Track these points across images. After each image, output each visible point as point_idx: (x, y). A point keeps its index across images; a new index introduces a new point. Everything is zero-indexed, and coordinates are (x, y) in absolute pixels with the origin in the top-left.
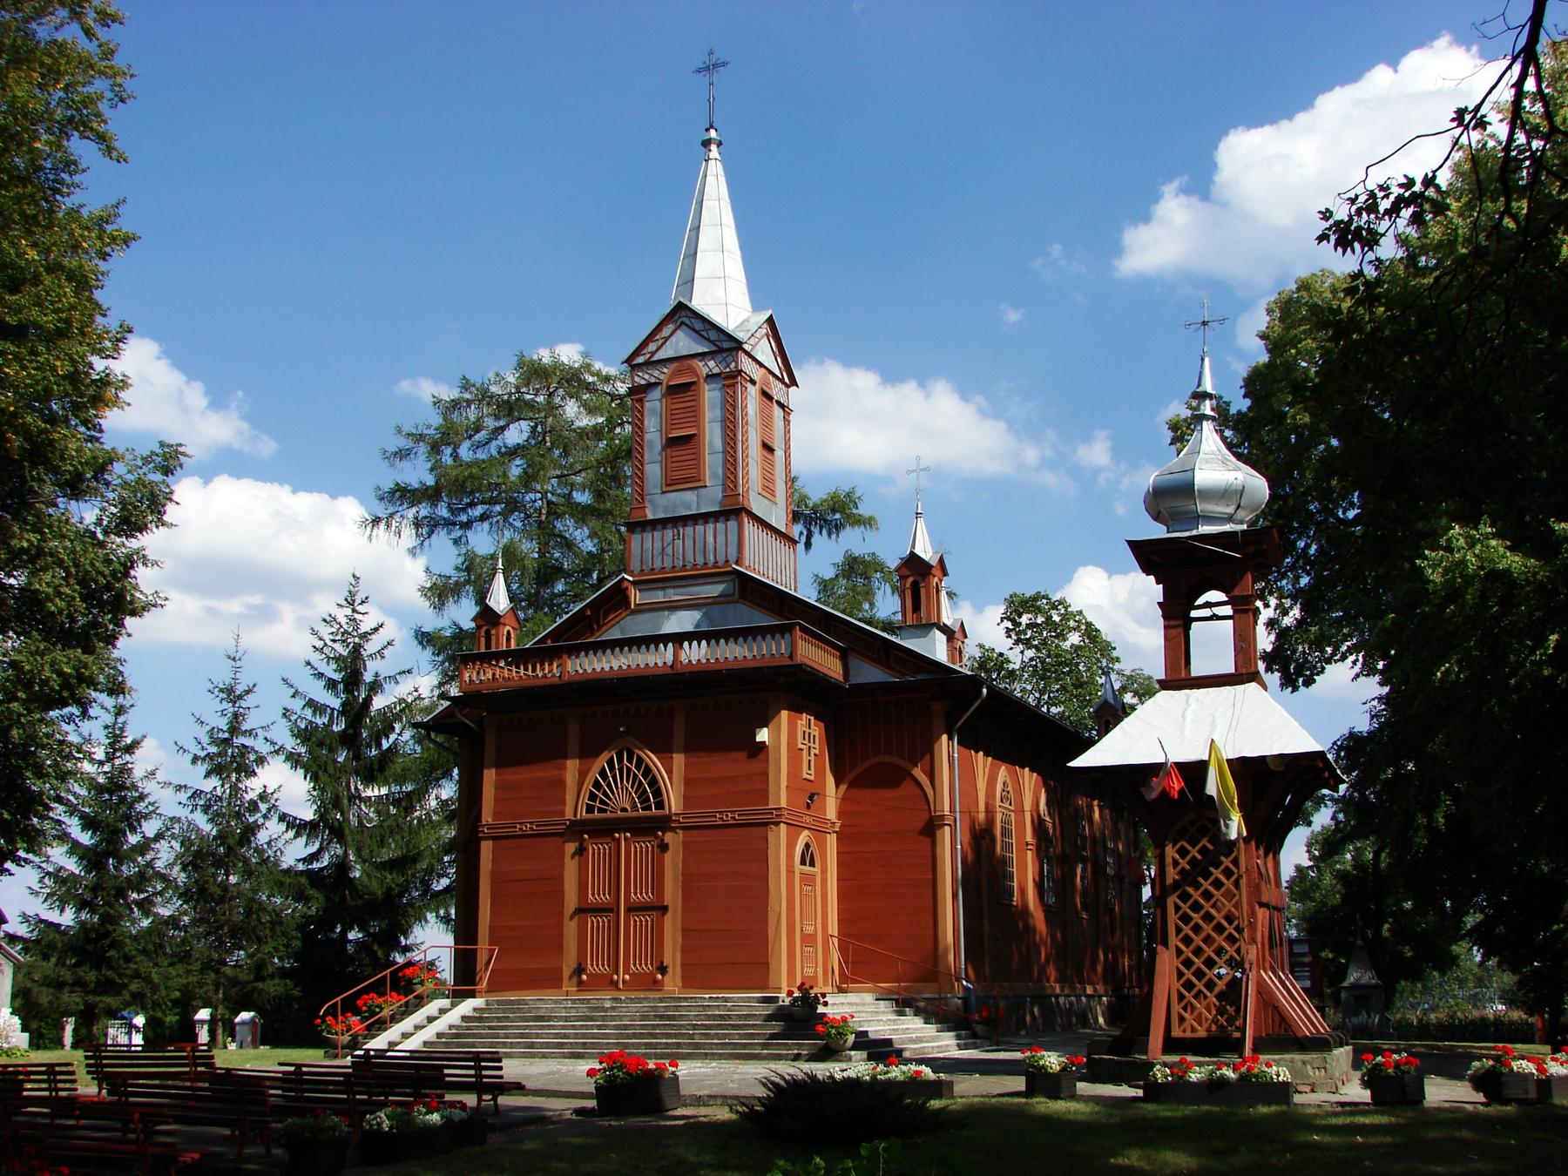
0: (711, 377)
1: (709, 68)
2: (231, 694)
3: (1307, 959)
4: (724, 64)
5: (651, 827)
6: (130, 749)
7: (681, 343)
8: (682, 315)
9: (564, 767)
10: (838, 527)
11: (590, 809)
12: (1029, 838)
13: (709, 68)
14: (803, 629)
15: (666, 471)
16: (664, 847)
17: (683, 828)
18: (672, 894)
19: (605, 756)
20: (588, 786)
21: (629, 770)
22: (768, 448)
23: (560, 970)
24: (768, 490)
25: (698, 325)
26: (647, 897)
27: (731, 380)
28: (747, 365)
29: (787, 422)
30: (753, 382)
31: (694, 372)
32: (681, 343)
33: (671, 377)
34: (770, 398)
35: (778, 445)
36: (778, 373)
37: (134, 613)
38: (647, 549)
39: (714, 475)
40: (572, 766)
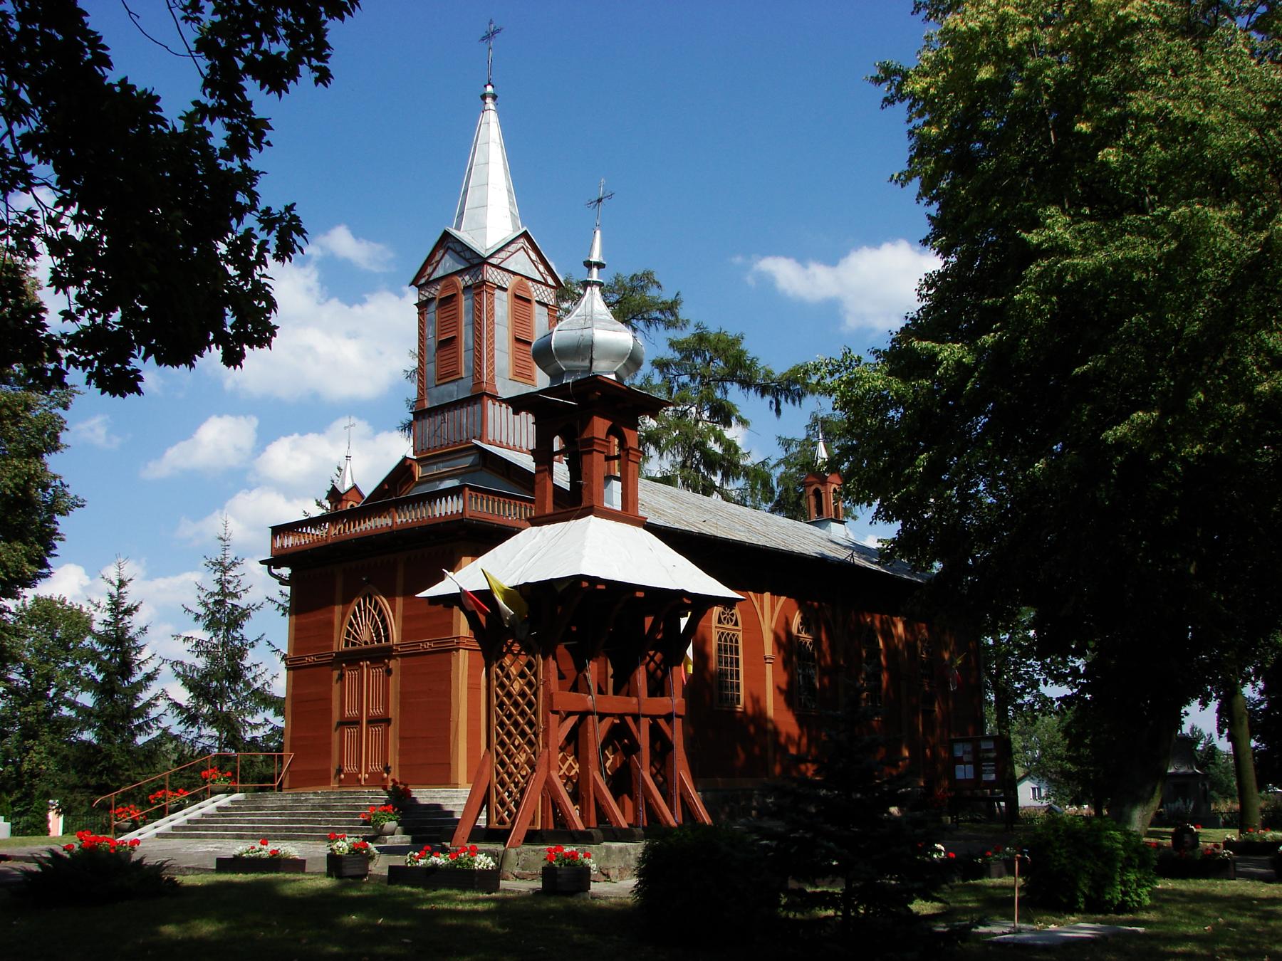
0: (467, 288)
1: (489, 37)
2: (223, 567)
3: (993, 755)
4: (498, 31)
5: (379, 655)
6: (129, 612)
7: (448, 264)
8: (447, 242)
9: (333, 612)
10: (800, 396)
11: (347, 645)
12: (769, 649)
13: (489, 37)
14: (472, 488)
15: (439, 367)
16: (389, 672)
17: (402, 656)
18: (394, 712)
19: (356, 601)
23: (328, 770)
26: (378, 711)
31: (455, 285)
32: (448, 264)
33: (442, 293)
36: (539, 278)
37: (64, 513)
39: (467, 368)
40: (338, 609)
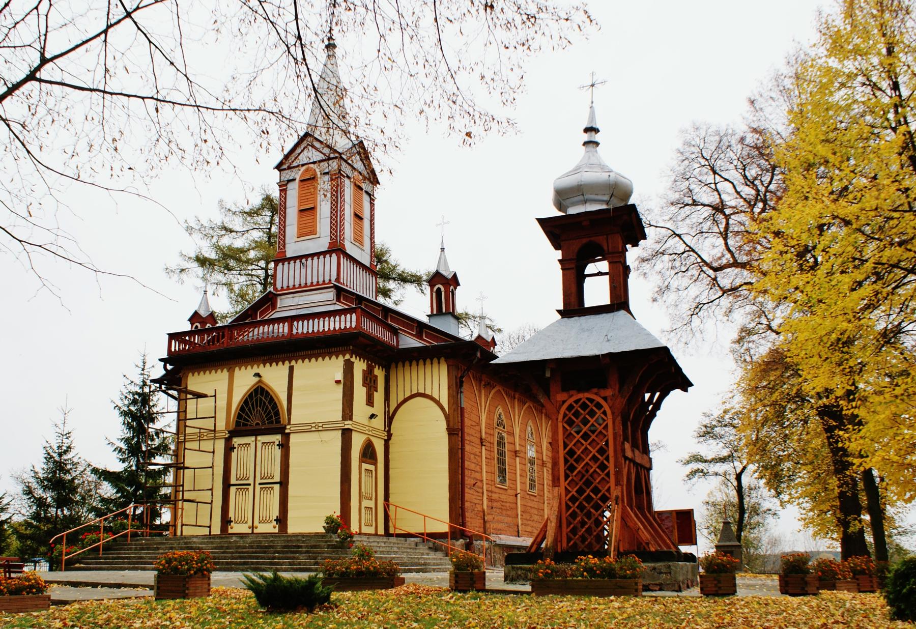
21: (261, 399)
22: (358, 217)
24: (358, 240)
29: (372, 205)
30: (348, 177)
34: (361, 189)
38: (286, 275)
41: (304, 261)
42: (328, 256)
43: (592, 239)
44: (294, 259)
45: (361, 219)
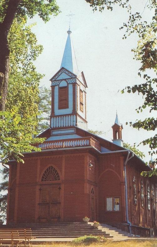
20: (43, 172)
25: (67, 72)
27: (74, 84)
28: (78, 82)
32: (64, 76)
35: (84, 103)
41: (62, 117)
42: (72, 116)
43: (82, 137)
44: (58, 116)
45: (83, 105)
